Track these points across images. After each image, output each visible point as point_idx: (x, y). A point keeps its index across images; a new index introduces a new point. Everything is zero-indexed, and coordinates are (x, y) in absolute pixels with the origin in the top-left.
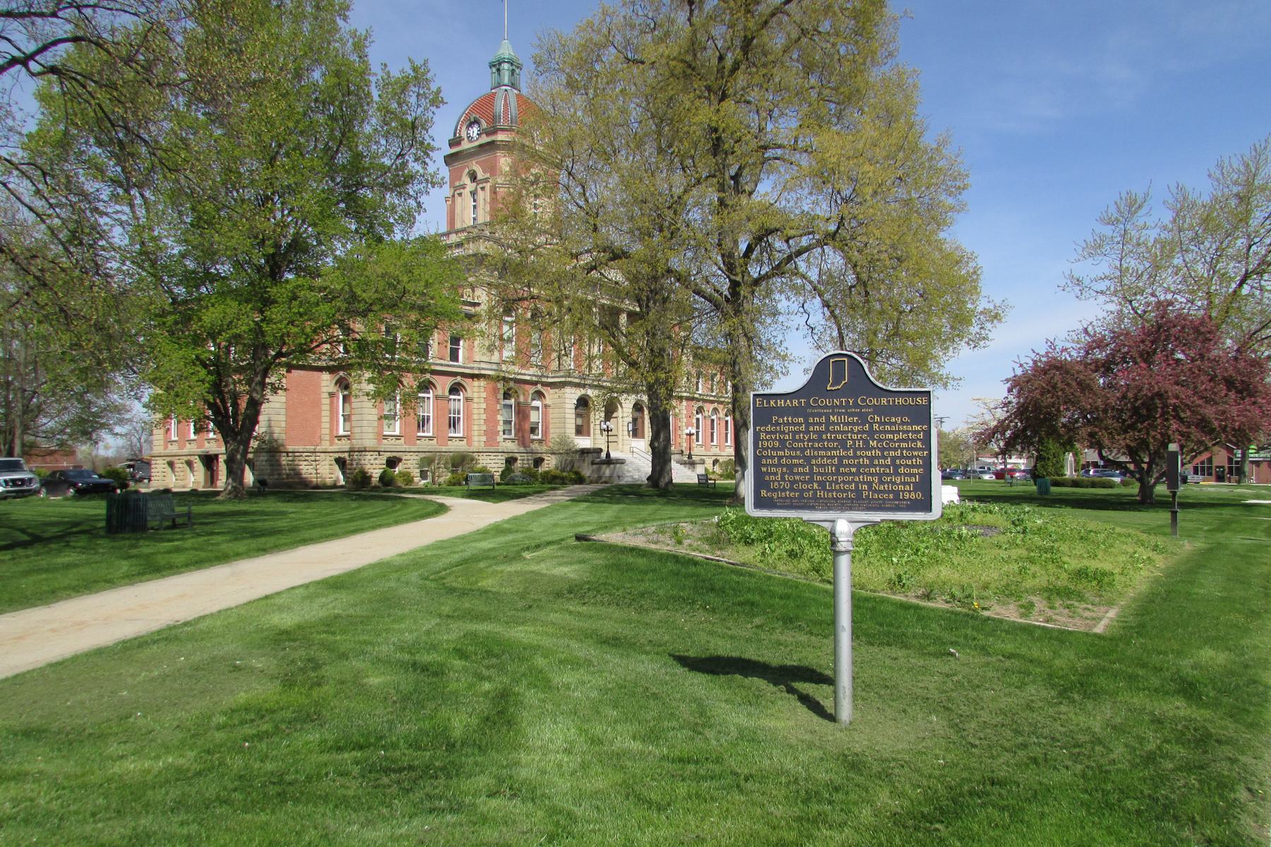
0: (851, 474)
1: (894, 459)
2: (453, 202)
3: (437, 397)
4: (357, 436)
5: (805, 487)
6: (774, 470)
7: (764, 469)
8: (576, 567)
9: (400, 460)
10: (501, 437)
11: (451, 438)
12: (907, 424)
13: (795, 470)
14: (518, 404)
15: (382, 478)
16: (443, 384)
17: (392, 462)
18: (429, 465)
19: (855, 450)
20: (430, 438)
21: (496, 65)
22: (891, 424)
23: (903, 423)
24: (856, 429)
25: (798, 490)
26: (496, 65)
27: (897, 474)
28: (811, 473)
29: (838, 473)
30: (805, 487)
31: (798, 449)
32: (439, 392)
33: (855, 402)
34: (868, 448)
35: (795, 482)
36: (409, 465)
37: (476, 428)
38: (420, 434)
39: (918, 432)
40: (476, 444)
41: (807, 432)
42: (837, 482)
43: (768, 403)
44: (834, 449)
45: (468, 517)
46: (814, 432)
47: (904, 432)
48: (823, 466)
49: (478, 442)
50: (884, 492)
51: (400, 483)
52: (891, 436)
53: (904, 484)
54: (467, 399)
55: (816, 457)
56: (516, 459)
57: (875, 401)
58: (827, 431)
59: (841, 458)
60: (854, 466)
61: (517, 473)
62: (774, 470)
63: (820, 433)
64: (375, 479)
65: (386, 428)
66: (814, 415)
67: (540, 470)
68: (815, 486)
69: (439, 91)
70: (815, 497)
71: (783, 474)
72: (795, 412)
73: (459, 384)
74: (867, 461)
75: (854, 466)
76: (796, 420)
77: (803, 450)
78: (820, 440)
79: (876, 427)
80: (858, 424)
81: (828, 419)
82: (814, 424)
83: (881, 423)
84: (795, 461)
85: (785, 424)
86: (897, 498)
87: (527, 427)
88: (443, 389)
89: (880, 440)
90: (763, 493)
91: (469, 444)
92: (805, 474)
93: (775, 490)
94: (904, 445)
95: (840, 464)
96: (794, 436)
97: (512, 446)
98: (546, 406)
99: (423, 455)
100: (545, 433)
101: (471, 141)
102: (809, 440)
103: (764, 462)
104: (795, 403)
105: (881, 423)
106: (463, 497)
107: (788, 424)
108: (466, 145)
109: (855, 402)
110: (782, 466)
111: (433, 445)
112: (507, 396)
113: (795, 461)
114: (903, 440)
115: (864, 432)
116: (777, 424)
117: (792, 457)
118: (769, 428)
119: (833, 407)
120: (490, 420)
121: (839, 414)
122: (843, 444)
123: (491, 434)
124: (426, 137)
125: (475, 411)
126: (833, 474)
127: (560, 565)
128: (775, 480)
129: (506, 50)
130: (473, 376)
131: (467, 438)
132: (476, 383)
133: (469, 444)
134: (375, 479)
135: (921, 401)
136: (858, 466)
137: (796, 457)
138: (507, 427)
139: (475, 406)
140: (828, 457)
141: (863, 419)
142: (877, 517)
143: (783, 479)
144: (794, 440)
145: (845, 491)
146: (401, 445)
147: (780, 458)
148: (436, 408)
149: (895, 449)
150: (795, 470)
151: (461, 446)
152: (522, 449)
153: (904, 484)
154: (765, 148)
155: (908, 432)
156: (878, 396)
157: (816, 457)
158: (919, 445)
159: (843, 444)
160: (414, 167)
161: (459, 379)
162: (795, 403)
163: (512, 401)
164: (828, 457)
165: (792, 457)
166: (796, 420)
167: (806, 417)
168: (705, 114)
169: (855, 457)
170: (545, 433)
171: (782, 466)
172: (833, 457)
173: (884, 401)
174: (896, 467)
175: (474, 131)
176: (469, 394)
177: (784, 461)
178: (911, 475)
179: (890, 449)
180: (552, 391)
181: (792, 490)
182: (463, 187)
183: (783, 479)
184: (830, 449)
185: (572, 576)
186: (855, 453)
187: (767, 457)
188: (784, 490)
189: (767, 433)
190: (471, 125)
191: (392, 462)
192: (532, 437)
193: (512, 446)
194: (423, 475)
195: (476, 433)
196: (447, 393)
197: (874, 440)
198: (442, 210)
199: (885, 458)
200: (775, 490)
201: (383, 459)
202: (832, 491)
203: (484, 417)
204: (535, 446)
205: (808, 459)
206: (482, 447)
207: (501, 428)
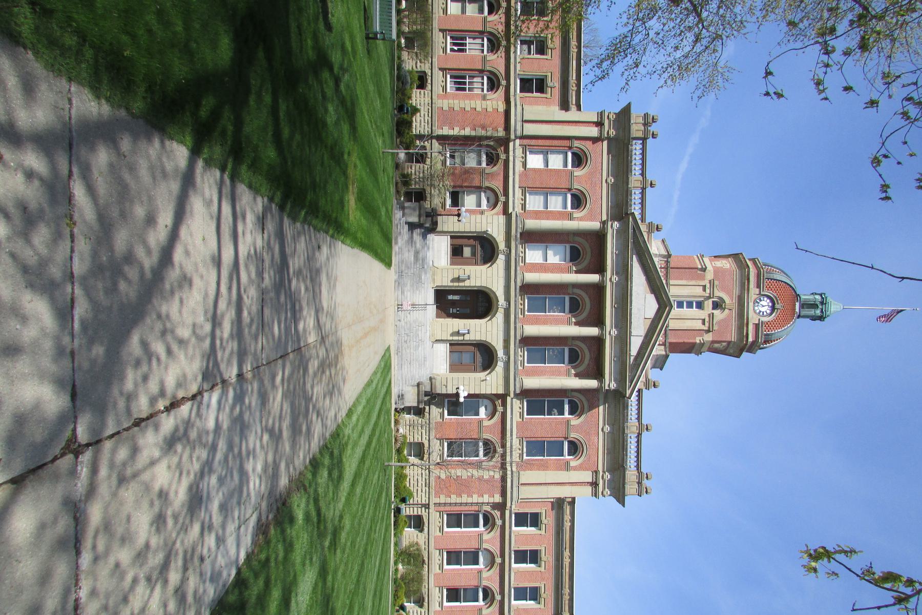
99: (426, 445)
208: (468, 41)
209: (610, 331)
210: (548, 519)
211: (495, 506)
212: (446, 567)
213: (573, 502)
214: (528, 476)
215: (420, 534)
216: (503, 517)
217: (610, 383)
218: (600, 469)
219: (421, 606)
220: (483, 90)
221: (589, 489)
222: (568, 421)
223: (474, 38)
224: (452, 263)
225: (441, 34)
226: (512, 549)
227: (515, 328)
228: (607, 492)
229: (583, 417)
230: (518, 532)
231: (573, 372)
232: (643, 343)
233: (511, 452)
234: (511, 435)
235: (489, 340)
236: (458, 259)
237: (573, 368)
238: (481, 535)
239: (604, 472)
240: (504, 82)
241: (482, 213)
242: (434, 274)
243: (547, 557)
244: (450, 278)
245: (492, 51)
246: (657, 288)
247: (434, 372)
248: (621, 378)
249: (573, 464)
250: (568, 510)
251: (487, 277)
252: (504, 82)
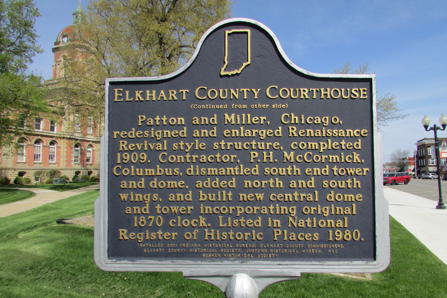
0: (257, 202)
1: (320, 178)
2: (56, 67)
3: (44, 146)
4: (4, 163)
5: (186, 223)
6: (139, 197)
7: (124, 196)
8: (45, 245)
9: (25, 173)
10: (73, 163)
11: (50, 164)
12: (339, 126)
13: (172, 197)
14: (81, 149)
15: (16, 181)
16: (47, 141)
17: (21, 174)
18: (39, 175)
19: (263, 165)
20: (40, 164)
21: (75, 14)
22: (315, 126)
23: (332, 125)
24: (264, 133)
25: (176, 229)
26: (75, 14)
27: (324, 202)
28: (196, 202)
29: (236, 201)
30: (186, 223)
31: (175, 164)
32: (45, 144)
33: (263, 94)
34: (281, 162)
35: (172, 215)
36: (30, 175)
37: (62, 159)
38: (36, 162)
39: (354, 139)
40: (62, 166)
41: (191, 138)
42: (234, 216)
43: (132, 94)
44: (230, 164)
45: (45, 197)
46: (201, 138)
47: (334, 138)
48: (213, 190)
49: (63, 165)
50: (306, 229)
51: (24, 183)
52: (314, 145)
53: (335, 217)
54: (58, 147)
55: (203, 177)
56: (80, 172)
57: (291, 93)
58: (221, 137)
59: (241, 178)
60: (261, 190)
61: (80, 178)
62: (139, 197)
63: (210, 140)
64: (12, 182)
65: (18, 159)
66: (200, 113)
67: (91, 176)
68: (202, 221)
69: (37, 9)
70: (202, 241)
71: (153, 203)
72: (172, 108)
73: (54, 141)
74: (280, 183)
75: (261, 190)
76: (174, 120)
77: (183, 166)
78: (210, 150)
79: (293, 131)
80: (266, 127)
81: (221, 118)
82: (201, 126)
83: (300, 126)
84: (172, 183)
85: (157, 127)
86: (324, 239)
87: (85, 159)
88: (47, 143)
89: (299, 151)
90: (123, 233)
91: (59, 166)
92: (186, 203)
93: (140, 229)
94: (335, 158)
95: (240, 188)
96: (170, 145)
97: (78, 167)
98: (94, 151)
99: (37, 171)
100: (93, 161)
101: (64, 43)
102: (193, 151)
103: (124, 184)
104: (173, 94)
105: (300, 126)
106: (48, 189)
107: (162, 127)
108: (61, 45)
109: (263, 94)
110: (152, 190)
111: (42, 166)
112: (76, 146)
113: (172, 183)
114: (333, 151)
115: (276, 138)
116: (146, 126)
117: (167, 177)
118: (133, 133)
119: (230, 101)
120: (69, 156)
121: (239, 111)
122: (243, 155)
123: (68, 162)
124: (33, 30)
125: (62, 152)
126: (228, 203)
127: (35, 244)
128: (140, 215)
129: (79, 9)
130: (60, 138)
131: (58, 163)
132: (62, 141)
133: (59, 166)
134: (12, 182)
135: (359, 92)
136: (267, 190)
137: (174, 177)
138: (77, 159)
139: (62, 150)
140: (221, 177)
141: (274, 120)
142: (296, 269)
143: (153, 211)
144: (171, 151)
145: (247, 229)
146: (26, 166)
147: (150, 178)
148: (44, 151)
149: (322, 165)
150: (172, 197)
151: (55, 167)
152: (83, 168)
153: (335, 217)
154: (181, 47)
155: (340, 138)
156: (296, 86)
157: (203, 177)
158: (356, 157)
159: (244, 156)
160: (29, 44)
161: (40, 137)
162: (173, 94)
163: (79, 148)
164: (221, 177)
165: (167, 177)
166: (174, 120)
167: (189, 117)
168: (156, 26)
169: (263, 176)
170: (93, 161)
171: (152, 190)
172: (229, 177)
173: (305, 92)
174: (324, 191)
175: (65, 39)
176: (59, 145)
177: (154, 183)
178: (346, 203)
179: (314, 164)
180: (96, 144)
181: (166, 228)
182: (60, 61)
183: (153, 211)
184: (223, 164)
185: (40, 253)
186: (262, 170)
187: (130, 177)
188: (155, 228)
189: (130, 140)
190: (64, 37)
191: (21, 174)
192: (88, 163)
193: (78, 167)
194: (37, 179)
195: (62, 161)
196: (49, 145)
197: (289, 150)
198: (42, 67)
199: (307, 177)
200: (140, 229)
201: (17, 172)
202: (227, 229)
203: (66, 155)
204: (89, 167)
205: (191, 180)
206: (64, 167)
207: (73, 159)
220: (54, 148)
241: (94, 151)
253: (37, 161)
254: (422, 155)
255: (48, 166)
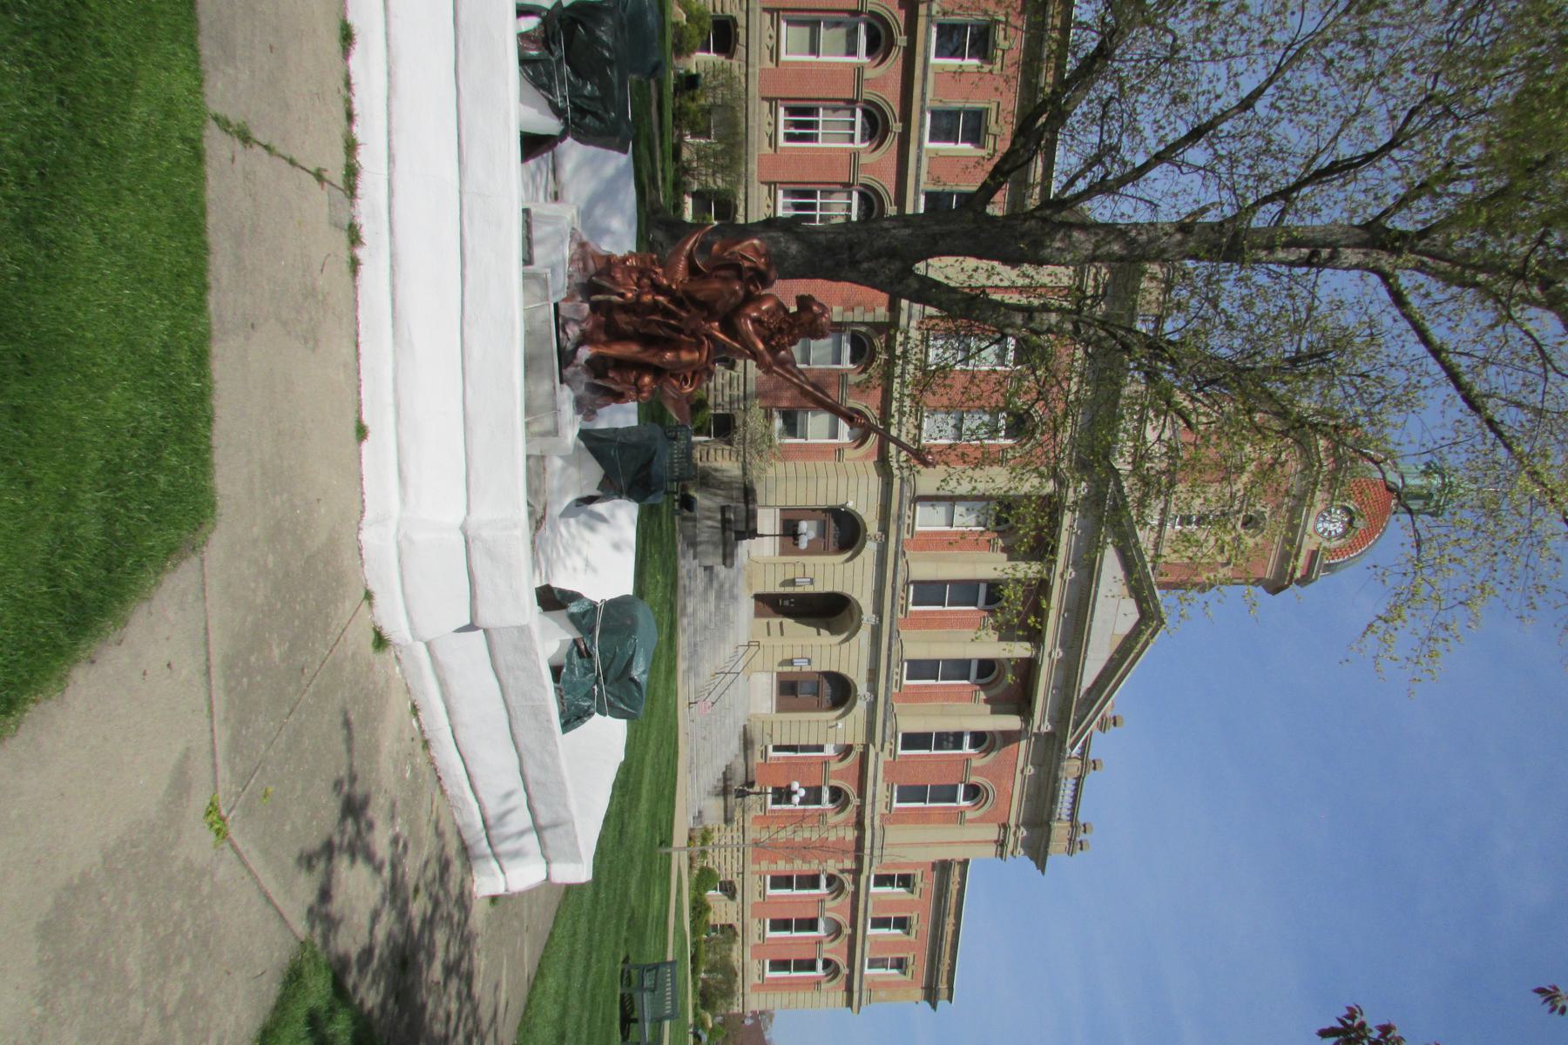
73: (847, 802)
88: (830, 951)
91: (756, 988)
99: (742, 21)
133: (756, 988)
170: (786, 454)
208: (821, 117)
209: (1051, 651)
210: (926, 882)
211: (877, 327)
212: (769, 892)
213: (965, 863)
214: (895, 834)
215: (730, 903)
216: (856, 882)
217: (1041, 722)
218: (1012, 822)
219: (732, 897)
220: (852, 139)
221: (993, 848)
222: (967, 759)
223: (835, 110)
224: (781, 708)
225: (766, 105)
226: (922, 186)
227: (890, 649)
228: (1020, 850)
229: (993, 754)
230: (937, 151)
231: (982, 695)
232: (1105, 669)
233: (873, 803)
234: (918, 168)
235: (843, 671)
236: (790, 700)
237: (983, 687)
238: (860, 69)
239: (1017, 826)
240: (902, 40)
241: (839, 450)
242: (750, 577)
243: (921, 925)
244: (780, 579)
245: (871, 138)
246: (1139, 590)
247: (752, 711)
248: (1061, 717)
249: (969, 815)
250: (956, 871)
251: (846, 575)
252: (897, 127)
253: (788, 124)
254: (718, 9)
255: (753, 916)
